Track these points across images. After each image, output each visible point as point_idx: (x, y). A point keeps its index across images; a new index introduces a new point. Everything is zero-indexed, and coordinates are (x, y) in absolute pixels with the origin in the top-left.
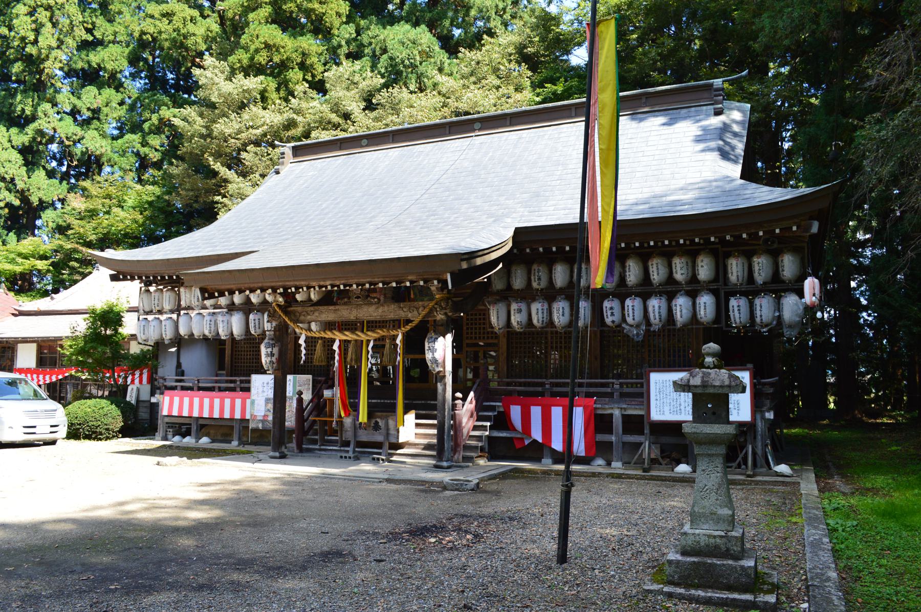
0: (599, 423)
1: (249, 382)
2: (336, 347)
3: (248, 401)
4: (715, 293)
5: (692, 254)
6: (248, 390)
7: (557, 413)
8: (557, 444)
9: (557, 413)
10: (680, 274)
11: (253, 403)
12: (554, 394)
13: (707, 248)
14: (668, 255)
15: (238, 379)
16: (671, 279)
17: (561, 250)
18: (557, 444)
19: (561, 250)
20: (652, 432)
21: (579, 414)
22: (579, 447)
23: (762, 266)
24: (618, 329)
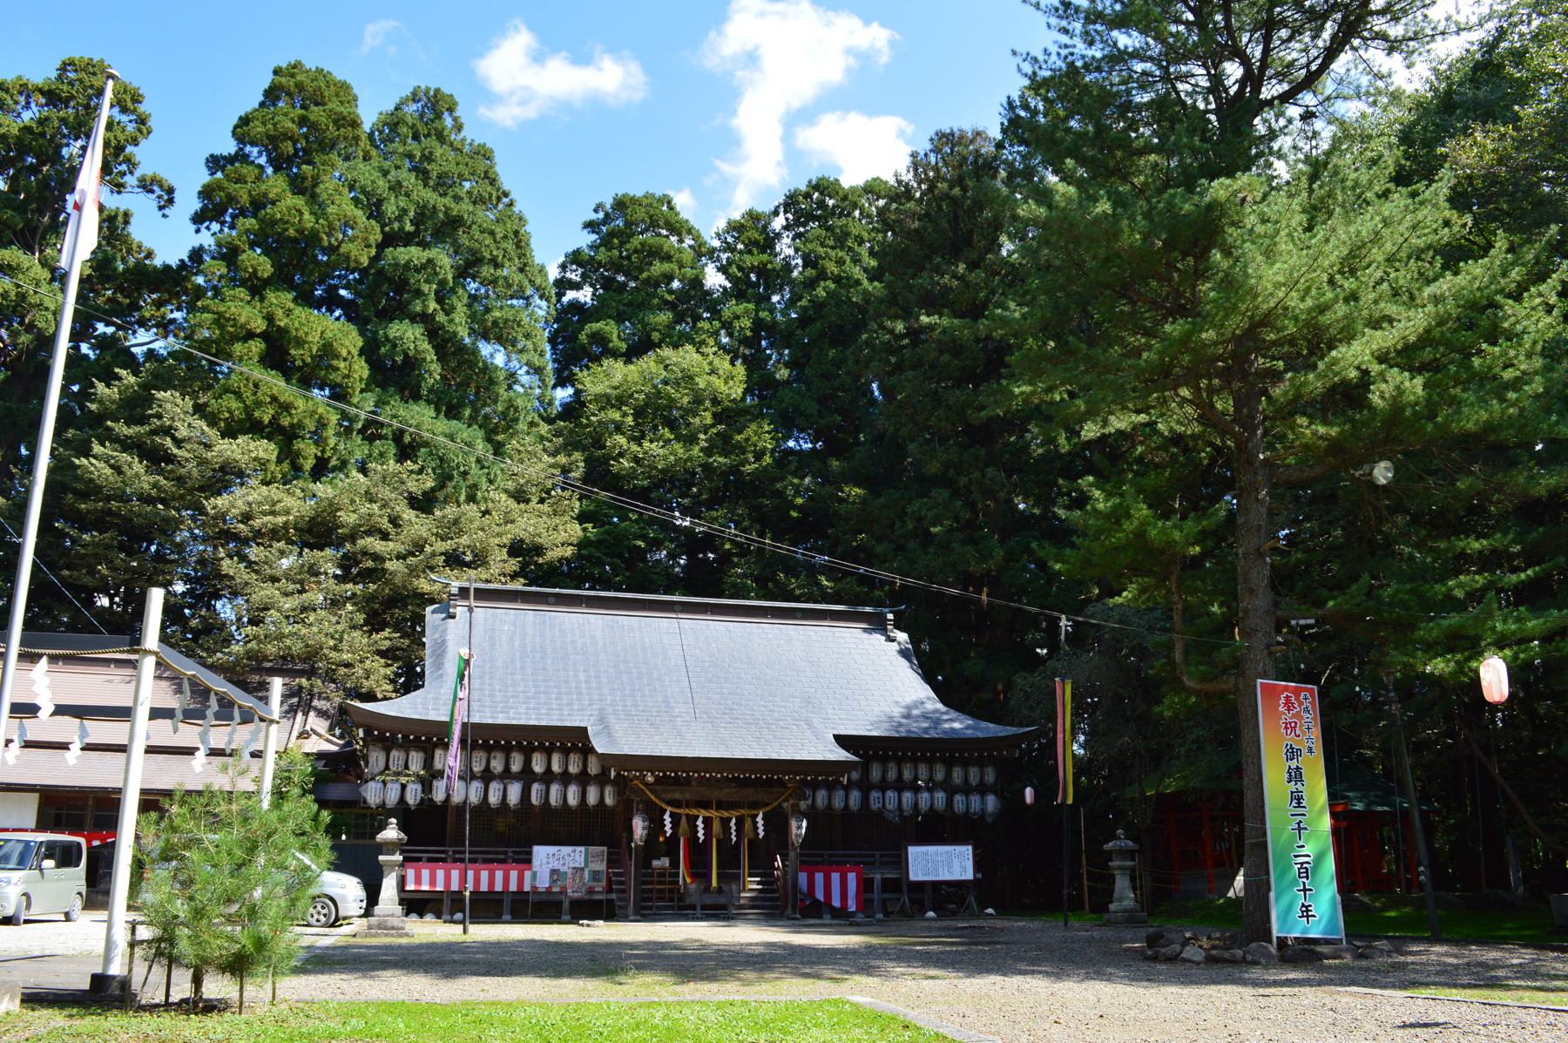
0: (865, 886)
1: (530, 853)
2: (732, 823)
3: (528, 874)
4: (861, 789)
5: (507, 750)
6: (529, 861)
7: (835, 877)
8: (836, 903)
9: (835, 877)
10: (556, 767)
11: (534, 874)
12: (832, 863)
13: (943, 760)
14: (965, 764)
15: (878, 854)
16: (487, 769)
17: (519, 743)
18: (836, 903)
19: (417, 738)
20: (909, 891)
21: (852, 877)
22: (852, 908)
23: (974, 774)
24: (879, 814)
